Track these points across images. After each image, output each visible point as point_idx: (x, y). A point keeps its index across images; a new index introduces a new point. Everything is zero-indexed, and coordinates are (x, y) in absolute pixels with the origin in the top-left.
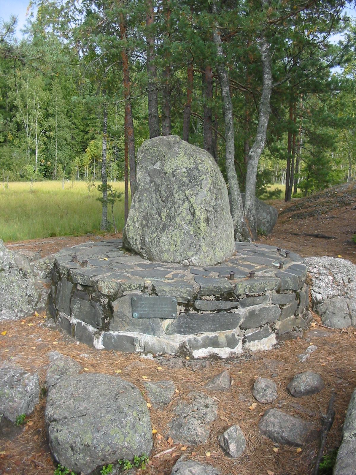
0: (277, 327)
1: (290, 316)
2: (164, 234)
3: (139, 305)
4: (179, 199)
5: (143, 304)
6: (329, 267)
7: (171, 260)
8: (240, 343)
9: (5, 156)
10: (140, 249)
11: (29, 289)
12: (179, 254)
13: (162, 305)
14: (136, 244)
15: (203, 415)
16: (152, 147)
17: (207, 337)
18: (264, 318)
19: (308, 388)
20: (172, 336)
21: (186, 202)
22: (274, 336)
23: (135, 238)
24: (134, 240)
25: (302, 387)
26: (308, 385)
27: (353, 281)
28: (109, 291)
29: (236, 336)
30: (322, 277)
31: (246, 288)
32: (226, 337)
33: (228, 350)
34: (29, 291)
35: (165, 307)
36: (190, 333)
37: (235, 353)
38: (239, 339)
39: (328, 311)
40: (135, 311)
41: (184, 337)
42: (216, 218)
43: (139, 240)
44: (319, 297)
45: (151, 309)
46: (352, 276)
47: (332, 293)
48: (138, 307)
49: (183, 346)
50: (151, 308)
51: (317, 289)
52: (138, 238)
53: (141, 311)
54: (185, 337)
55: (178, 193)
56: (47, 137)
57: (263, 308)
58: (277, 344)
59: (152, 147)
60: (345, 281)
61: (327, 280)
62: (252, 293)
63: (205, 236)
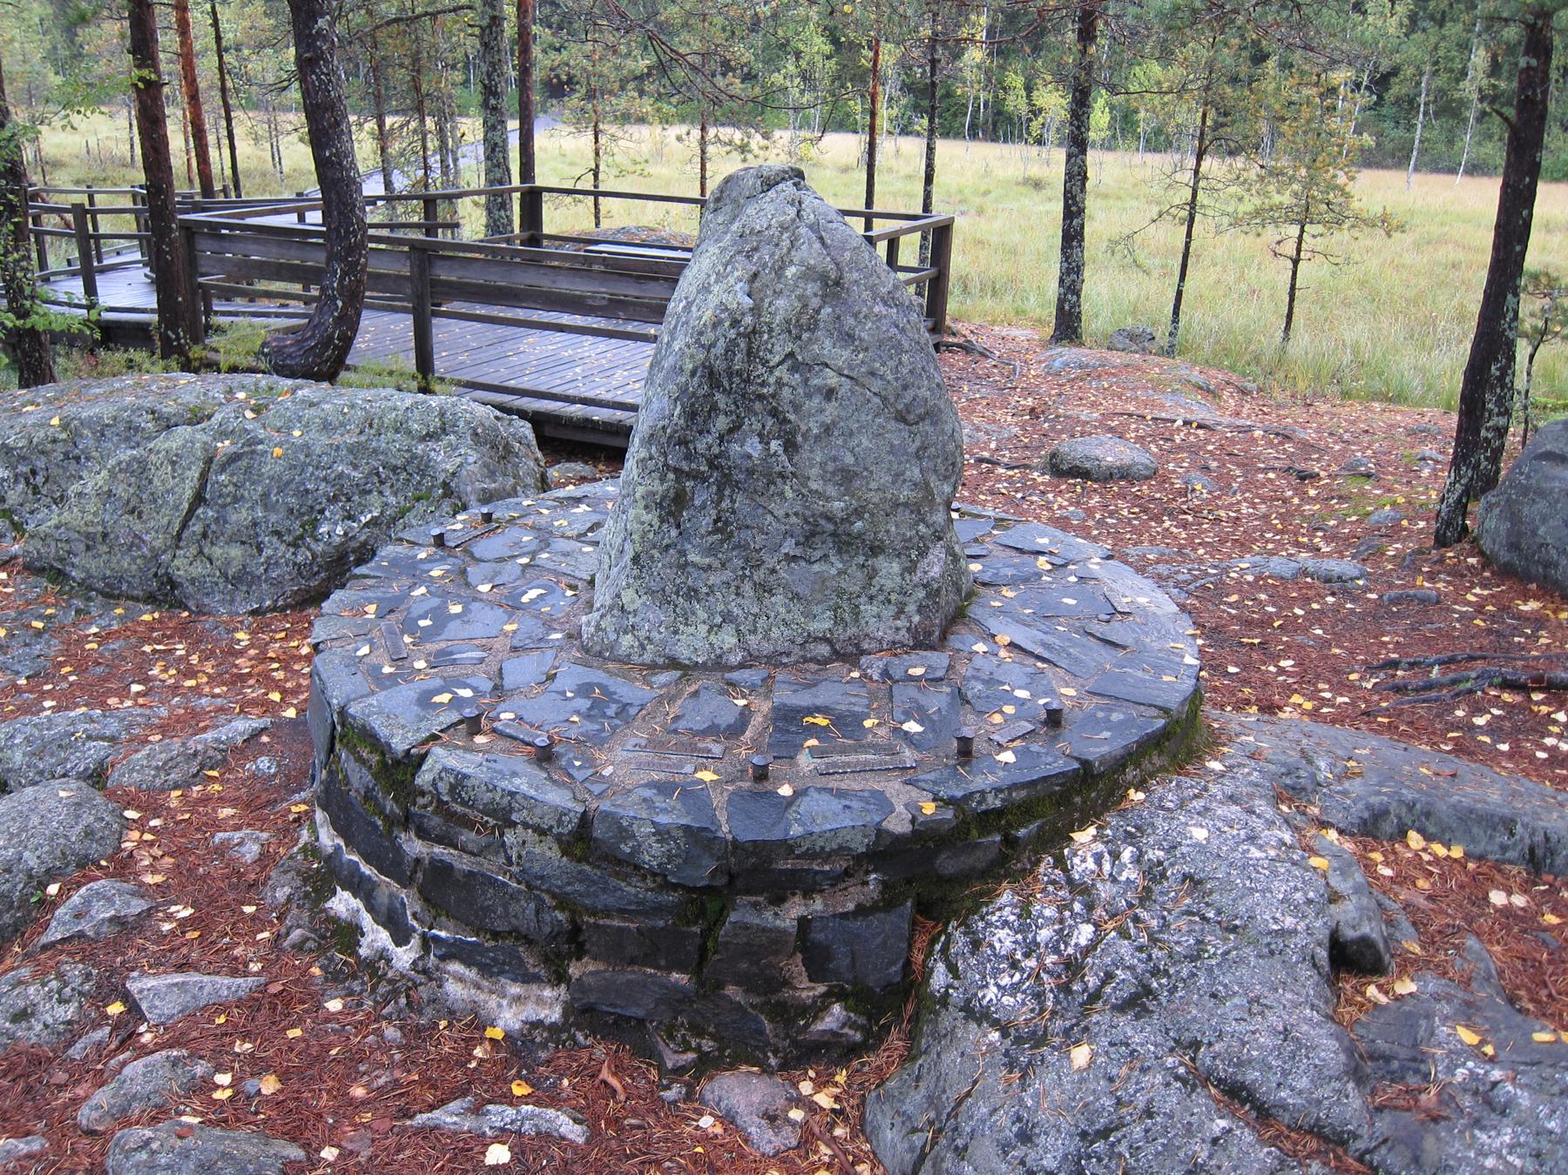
42: (725, 504)
44: (939, 978)
51: (960, 941)
57: (483, 875)
58: (553, 1028)
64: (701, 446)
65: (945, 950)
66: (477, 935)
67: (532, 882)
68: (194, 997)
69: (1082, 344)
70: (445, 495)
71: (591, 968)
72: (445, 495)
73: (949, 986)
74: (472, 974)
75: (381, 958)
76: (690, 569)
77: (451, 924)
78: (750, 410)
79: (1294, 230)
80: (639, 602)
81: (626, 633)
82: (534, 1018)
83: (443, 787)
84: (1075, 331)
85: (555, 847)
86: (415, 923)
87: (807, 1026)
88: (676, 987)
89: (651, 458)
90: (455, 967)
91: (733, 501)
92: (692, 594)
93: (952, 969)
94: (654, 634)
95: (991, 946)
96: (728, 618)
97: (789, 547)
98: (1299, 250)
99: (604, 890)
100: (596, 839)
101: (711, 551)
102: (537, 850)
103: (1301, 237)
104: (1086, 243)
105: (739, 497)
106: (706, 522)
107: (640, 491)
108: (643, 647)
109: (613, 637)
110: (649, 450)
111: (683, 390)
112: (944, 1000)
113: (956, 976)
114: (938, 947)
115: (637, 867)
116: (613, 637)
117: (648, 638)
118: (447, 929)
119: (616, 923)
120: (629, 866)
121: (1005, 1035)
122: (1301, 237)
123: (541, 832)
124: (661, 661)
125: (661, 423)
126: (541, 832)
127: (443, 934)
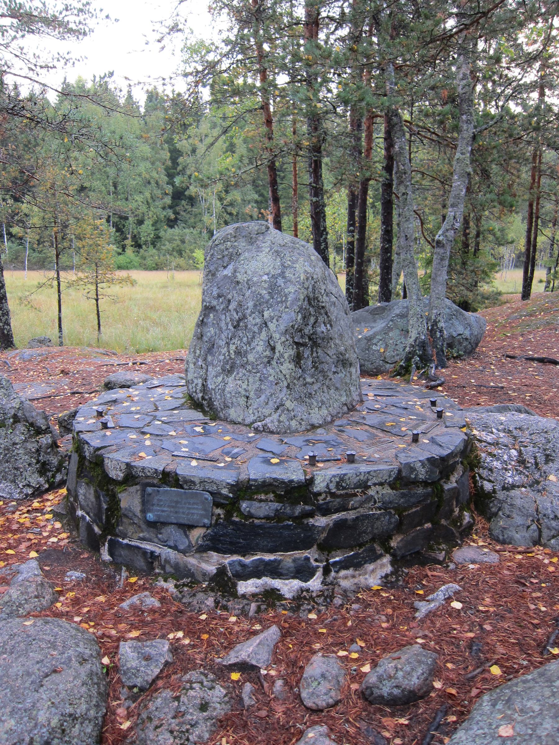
0: (393, 544)
1: (421, 524)
2: (231, 379)
3: (155, 502)
4: (255, 325)
5: (161, 500)
6: (515, 432)
7: (240, 420)
8: (319, 574)
9: (176, 240)
10: (200, 399)
11: (42, 454)
12: (251, 412)
13: (189, 503)
14: (196, 392)
15: (189, 727)
16: (224, 242)
17: (261, 560)
18: (365, 532)
19: (396, 691)
20: (205, 555)
21: (264, 329)
22: (386, 559)
23: (196, 381)
24: (194, 385)
25: (384, 688)
26: (397, 687)
27: (552, 461)
28: (117, 475)
29: (312, 561)
30: (500, 451)
31: (331, 482)
32: (294, 561)
33: (296, 584)
34: (43, 456)
35: (194, 508)
36: (232, 552)
37: (308, 590)
38: (318, 567)
39: (500, 513)
40: (150, 511)
41: (223, 557)
42: (315, 355)
43: (200, 385)
44: (488, 486)
45: (172, 509)
46: (554, 451)
47: (510, 480)
48: (153, 505)
49: (222, 571)
50: (173, 507)
51: (485, 473)
52: (200, 381)
53: (158, 511)
54: (226, 558)
55: (253, 315)
56: (228, 213)
57: (362, 516)
58: (392, 573)
59: (224, 242)
60: (539, 460)
61: (505, 457)
62: (343, 490)
63: (291, 384)
64: (306, 331)
65: (481, 477)
66: (353, 551)
67: (386, 506)
68: (268, 646)
69: (17, 349)
70: (15, 422)
71: (399, 539)
72: (15, 422)
73: (493, 486)
74: (350, 572)
75: (302, 591)
76: (307, 385)
77: (339, 552)
78: (320, 314)
79: (94, 288)
80: (293, 405)
81: (292, 420)
82: (383, 575)
83: (332, 487)
84: (12, 343)
85: (389, 488)
86: (317, 564)
87: (461, 524)
88: (428, 529)
89: (287, 340)
90: (343, 573)
91: (317, 353)
92: (310, 396)
93: (489, 481)
94: (303, 417)
95: (496, 468)
96: (323, 402)
97: (334, 369)
98: (97, 295)
99: (411, 497)
100: (405, 477)
101: (312, 376)
102: (384, 492)
103: (97, 290)
104: (8, 301)
105: (319, 350)
106: (310, 363)
107: (286, 356)
108: (300, 424)
109: (287, 423)
110: (285, 337)
111: (301, 308)
112: (494, 491)
113: (493, 482)
114: (478, 478)
115: (418, 482)
116: (287, 423)
117: (302, 419)
118: (338, 556)
119: (414, 510)
120: (415, 483)
121: (525, 487)
122: (97, 290)
123: (381, 484)
124: (309, 427)
125: (291, 324)
126: (381, 484)
127: (337, 559)
